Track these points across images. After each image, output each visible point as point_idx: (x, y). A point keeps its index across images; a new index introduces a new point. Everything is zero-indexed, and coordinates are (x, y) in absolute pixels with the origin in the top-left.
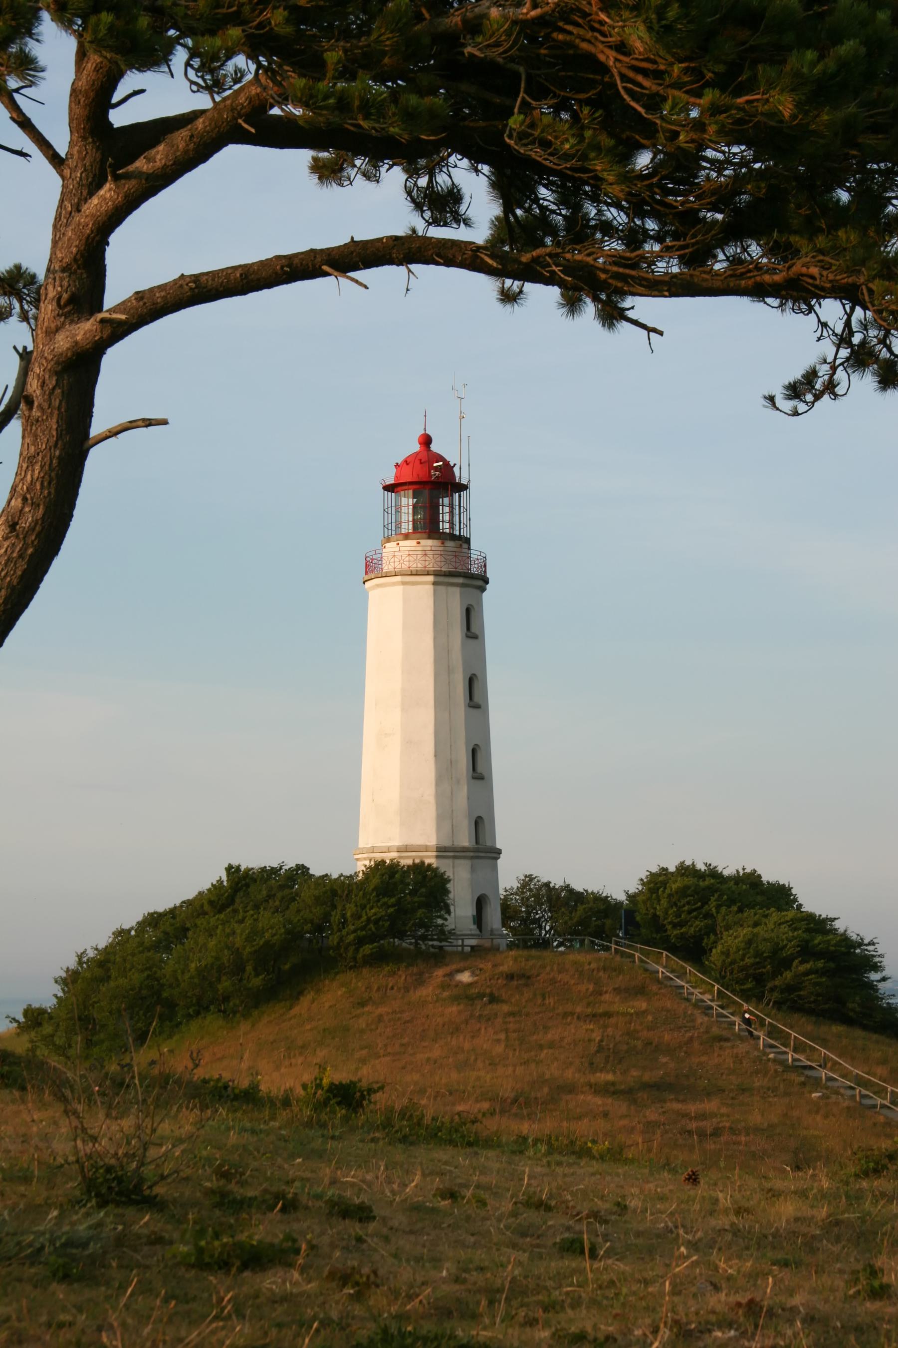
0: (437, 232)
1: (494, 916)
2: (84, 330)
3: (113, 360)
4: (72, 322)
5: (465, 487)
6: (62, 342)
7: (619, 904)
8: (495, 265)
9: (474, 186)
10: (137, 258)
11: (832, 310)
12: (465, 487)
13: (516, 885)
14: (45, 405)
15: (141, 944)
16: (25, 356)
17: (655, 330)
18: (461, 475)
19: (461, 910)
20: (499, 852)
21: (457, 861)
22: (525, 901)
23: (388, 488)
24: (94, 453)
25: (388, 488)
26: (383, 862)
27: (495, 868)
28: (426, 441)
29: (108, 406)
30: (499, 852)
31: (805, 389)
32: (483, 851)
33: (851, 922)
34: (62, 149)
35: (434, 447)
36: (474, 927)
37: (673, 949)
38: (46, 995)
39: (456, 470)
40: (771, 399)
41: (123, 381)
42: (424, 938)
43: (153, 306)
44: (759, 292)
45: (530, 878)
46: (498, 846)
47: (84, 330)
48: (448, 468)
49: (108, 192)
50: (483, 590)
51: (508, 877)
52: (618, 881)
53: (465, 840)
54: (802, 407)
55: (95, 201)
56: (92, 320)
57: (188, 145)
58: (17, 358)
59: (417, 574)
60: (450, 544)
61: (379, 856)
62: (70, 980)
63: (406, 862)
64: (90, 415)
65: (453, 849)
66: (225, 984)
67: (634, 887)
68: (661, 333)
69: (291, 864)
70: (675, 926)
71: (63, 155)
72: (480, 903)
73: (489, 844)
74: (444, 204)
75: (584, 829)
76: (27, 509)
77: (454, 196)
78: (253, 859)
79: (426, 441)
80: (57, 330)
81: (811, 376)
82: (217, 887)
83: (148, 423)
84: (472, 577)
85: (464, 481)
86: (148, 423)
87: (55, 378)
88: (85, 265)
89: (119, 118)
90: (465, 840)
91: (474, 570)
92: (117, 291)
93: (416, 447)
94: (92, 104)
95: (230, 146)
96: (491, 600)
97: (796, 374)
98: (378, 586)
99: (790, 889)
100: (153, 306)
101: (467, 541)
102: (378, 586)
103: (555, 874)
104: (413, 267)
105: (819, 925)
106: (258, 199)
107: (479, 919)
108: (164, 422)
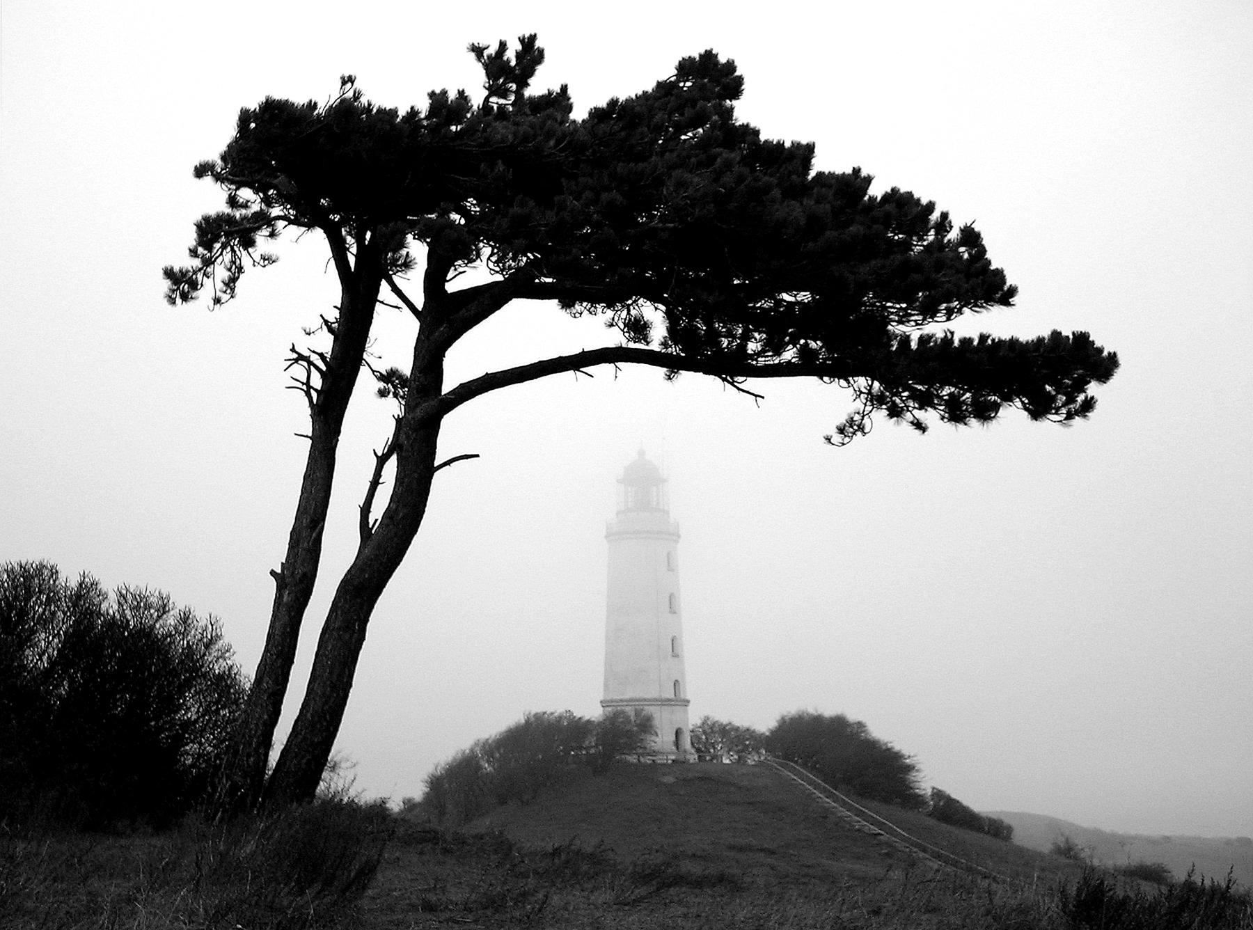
0: (632, 345)
3: (449, 422)
5: (665, 481)
6: (419, 413)
8: (274, 756)
9: (654, 315)
10: (460, 364)
11: (862, 382)
12: (665, 481)
13: (699, 722)
20: (688, 702)
22: (704, 732)
24: (437, 476)
27: (686, 712)
29: (445, 447)
30: (688, 702)
31: (851, 428)
33: (899, 745)
34: (419, 305)
40: (828, 439)
41: (454, 431)
42: (642, 755)
44: (820, 371)
45: (707, 718)
51: (693, 718)
54: (847, 440)
57: (484, 302)
72: (678, 733)
73: (682, 696)
74: (638, 328)
81: (851, 421)
89: (451, 287)
92: (449, 384)
94: (434, 280)
95: (514, 300)
97: (842, 420)
101: (668, 513)
103: (723, 716)
104: (618, 364)
106: (532, 326)
107: (677, 743)
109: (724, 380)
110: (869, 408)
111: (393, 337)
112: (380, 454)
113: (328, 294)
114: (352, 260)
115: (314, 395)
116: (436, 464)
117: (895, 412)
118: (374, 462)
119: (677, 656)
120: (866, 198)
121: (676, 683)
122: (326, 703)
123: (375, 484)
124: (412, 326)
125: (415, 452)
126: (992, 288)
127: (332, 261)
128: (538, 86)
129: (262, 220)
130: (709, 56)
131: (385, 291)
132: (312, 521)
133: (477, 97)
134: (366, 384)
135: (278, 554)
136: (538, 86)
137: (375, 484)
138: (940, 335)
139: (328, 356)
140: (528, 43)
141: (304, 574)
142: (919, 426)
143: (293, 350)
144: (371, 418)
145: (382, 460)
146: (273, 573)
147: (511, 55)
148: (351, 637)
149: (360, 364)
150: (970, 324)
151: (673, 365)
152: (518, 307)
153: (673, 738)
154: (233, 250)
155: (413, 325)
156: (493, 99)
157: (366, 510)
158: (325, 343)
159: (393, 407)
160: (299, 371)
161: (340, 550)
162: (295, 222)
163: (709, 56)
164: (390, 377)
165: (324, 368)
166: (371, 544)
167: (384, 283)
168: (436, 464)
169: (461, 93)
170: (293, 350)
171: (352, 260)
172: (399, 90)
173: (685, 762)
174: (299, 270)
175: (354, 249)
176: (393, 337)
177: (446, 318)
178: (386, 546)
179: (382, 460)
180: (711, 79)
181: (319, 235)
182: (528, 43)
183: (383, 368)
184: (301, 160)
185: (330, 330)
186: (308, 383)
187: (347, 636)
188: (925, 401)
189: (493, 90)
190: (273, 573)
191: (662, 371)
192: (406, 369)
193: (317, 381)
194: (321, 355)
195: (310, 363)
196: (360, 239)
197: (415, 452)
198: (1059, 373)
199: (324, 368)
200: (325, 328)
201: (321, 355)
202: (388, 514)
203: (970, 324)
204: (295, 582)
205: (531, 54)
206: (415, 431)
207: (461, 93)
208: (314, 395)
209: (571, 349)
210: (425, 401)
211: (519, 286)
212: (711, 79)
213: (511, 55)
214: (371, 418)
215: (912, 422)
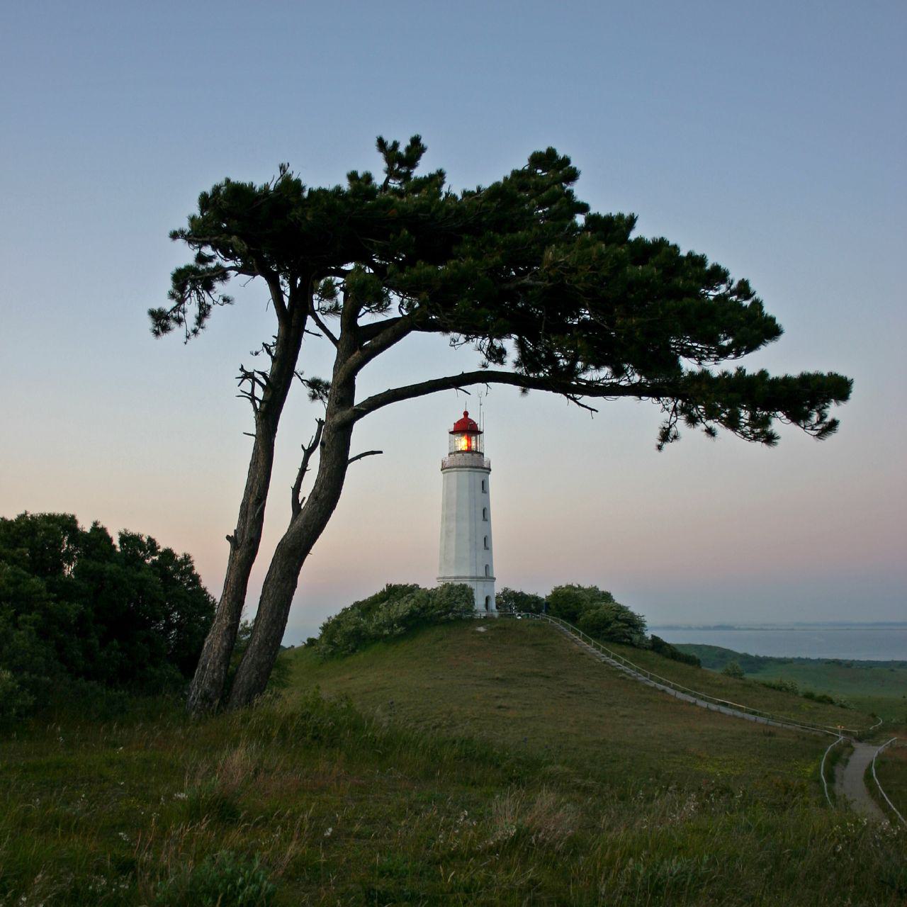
1: (493, 605)
2: (347, 413)
3: (359, 427)
4: (341, 410)
5: (481, 433)
6: (337, 418)
7: (543, 599)
10: (367, 383)
12: (481, 433)
13: (501, 592)
14: (330, 446)
15: (250, 252)
16: (321, 423)
17: (594, 410)
18: (480, 428)
19: (479, 603)
21: (478, 583)
23: (451, 433)
25: (451, 433)
26: (448, 583)
27: (493, 585)
28: (466, 414)
32: (488, 578)
35: (469, 417)
36: (485, 609)
37: (564, 618)
38: (316, 634)
39: (478, 426)
41: (363, 434)
43: (375, 403)
46: (494, 576)
47: (347, 413)
48: (475, 425)
49: (357, 354)
50: (489, 473)
51: (498, 588)
52: (544, 592)
53: (482, 573)
55: (351, 359)
56: (350, 409)
57: (390, 333)
58: (317, 423)
59: (462, 467)
60: (476, 455)
61: (447, 581)
62: (325, 628)
63: (457, 583)
64: (348, 449)
65: (477, 578)
66: (386, 632)
67: (549, 593)
68: (597, 411)
69: (411, 583)
70: (565, 608)
71: (338, 339)
72: (487, 599)
73: (491, 575)
74: (497, 355)
75: (526, 564)
76: (322, 491)
77: (502, 352)
78: (396, 581)
79: (466, 414)
80: (335, 413)
82: (383, 592)
83: (373, 453)
84: (485, 468)
85: (481, 430)
86: (373, 453)
87: (334, 435)
88: (345, 383)
90: (482, 573)
91: (485, 466)
92: (359, 398)
93: (463, 417)
96: (492, 479)
98: (447, 472)
99: (610, 594)
100: (375, 403)
101: (483, 454)
102: (447, 472)
105: (621, 609)
107: (487, 605)
108: (381, 452)
109: (568, 397)
110: (674, 419)
111: (318, 356)
112: (306, 448)
113: (270, 327)
114: (286, 300)
115: (258, 403)
116: (350, 458)
117: (692, 420)
118: (302, 454)
119: (488, 549)
120: (306, 194)
121: (487, 567)
122: (269, 634)
123: (303, 470)
124: (332, 352)
125: (335, 446)
126: (759, 329)
127: (272, 300)
128: (422, 170)
129: (222, 274)
130: (551, 153)
131: (310, 323)
132: (257, 499)
133: (379, 179)
134: (297, 391)
135: (231, 523)
136: (422, 170)
137: (303, 470)
138: (733, 371)
139: (268, 373)
140: (416, 141)
141: (252, 540)
142: (710, 432)
143: (242, 369)
144: (302, 416)
145: (308, 453)
146: (228, 538)
147: (402, 149)
148: (286, 586)
149: (291, 376)
150: (752, 363)
151: (524, 383)
152: (415, 338)
153: (484, 602)
154: (198, 293)
155: (333, 351)
156: (391, 181)
157: (296, 490)
158: (264, 364)
159: (320, 409)
160: (247, 385)
161: (277, 522)
162: (241, 270)
163: (551, 153)
164: (315, 384)
165: (265, 383)
166: (302, 517)
167: (309, 317)
168: (350, 458)
169: (353, 177)
170: (242, 369)
171: (286, 300)
172: (323, 175)
173: (493, 618)
174: (248, 304)
175: (288, 293)
176: (318, 356)
177: (358, 346)
178: (313, 518)
179: (308, 453)
180: (551, 170)
181: (260, 281)
182: (416, 141)
183: (307, 377)
184: (259, 229)
185: (269, 352)
186: (252, 394)
187: (284, 585)
188: (712, 414)
189: (391, 173)
190: (228, 538)
191: (517, 389)
192: (327, 376)
193: (259, 393)
194: (263, 374)
195: (255, 380)
196: (292, 283)
197: (335, 446)
198: (810, 397)
199: (265, 383)
200: (265, 349)
201: (263, 374)
202: (314, 495)
203: (752, 363)
204: (245, 543)
205: (416, 148)
206: (335, 432)
207: (353, 177)
208: (258, 403)
209: (455, 372)
210: (344, 409)
211: (415, 322)
212: (551, 170)
213: (402, 149)
214: (302, 416)
215: (706, 431)
